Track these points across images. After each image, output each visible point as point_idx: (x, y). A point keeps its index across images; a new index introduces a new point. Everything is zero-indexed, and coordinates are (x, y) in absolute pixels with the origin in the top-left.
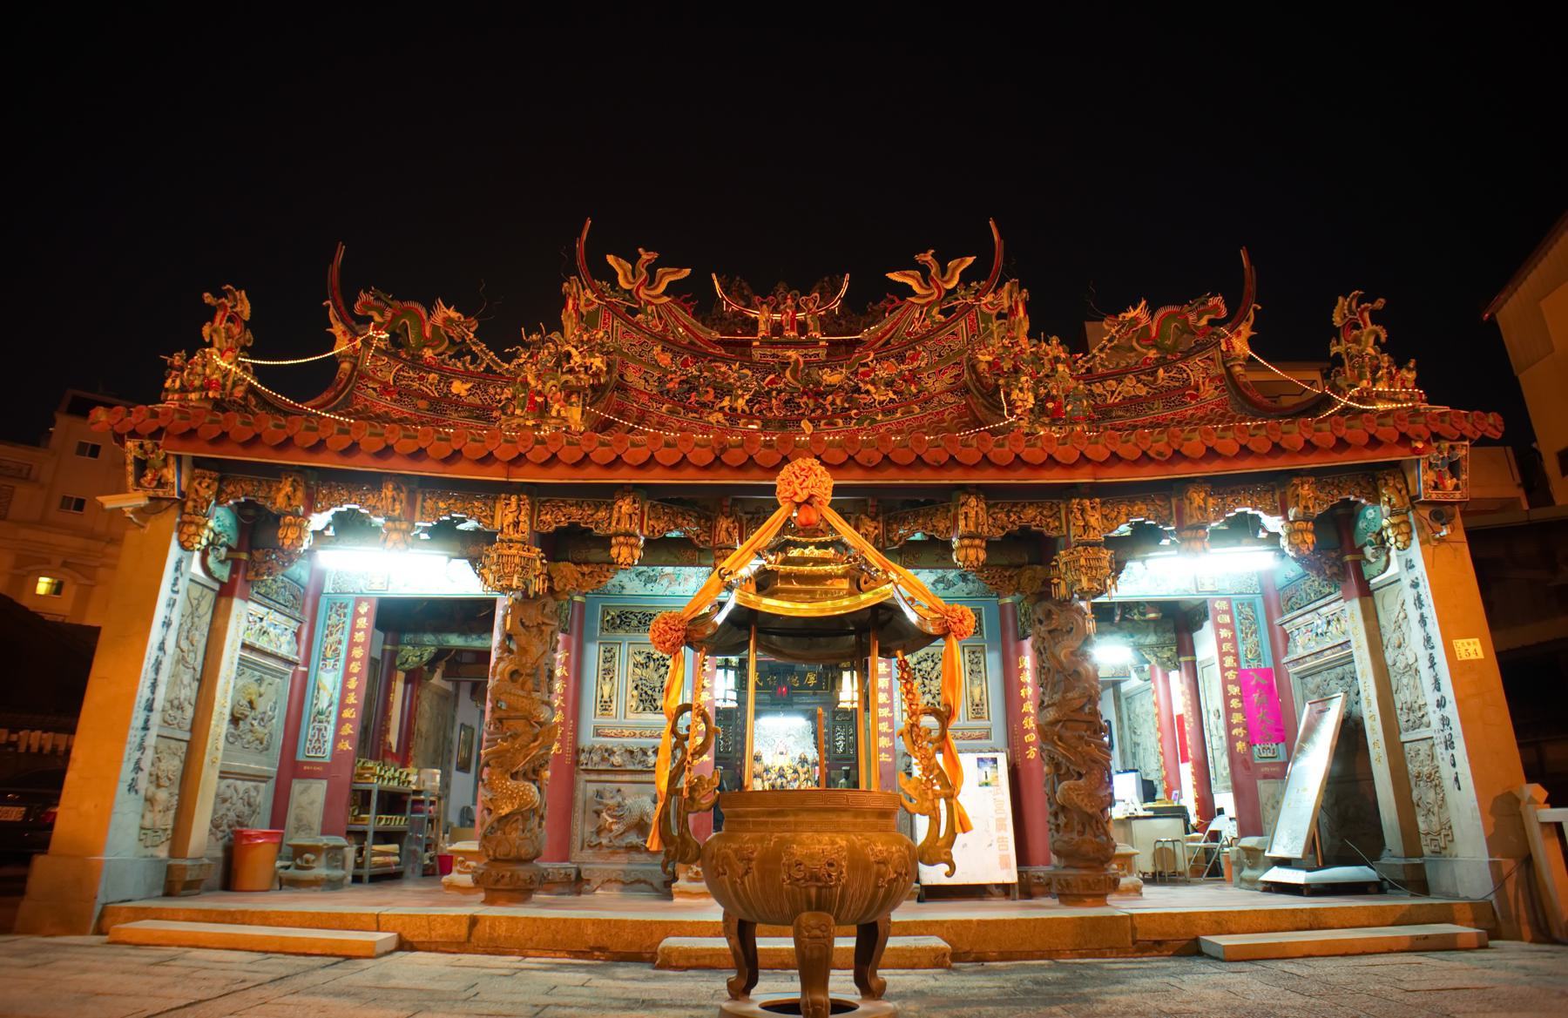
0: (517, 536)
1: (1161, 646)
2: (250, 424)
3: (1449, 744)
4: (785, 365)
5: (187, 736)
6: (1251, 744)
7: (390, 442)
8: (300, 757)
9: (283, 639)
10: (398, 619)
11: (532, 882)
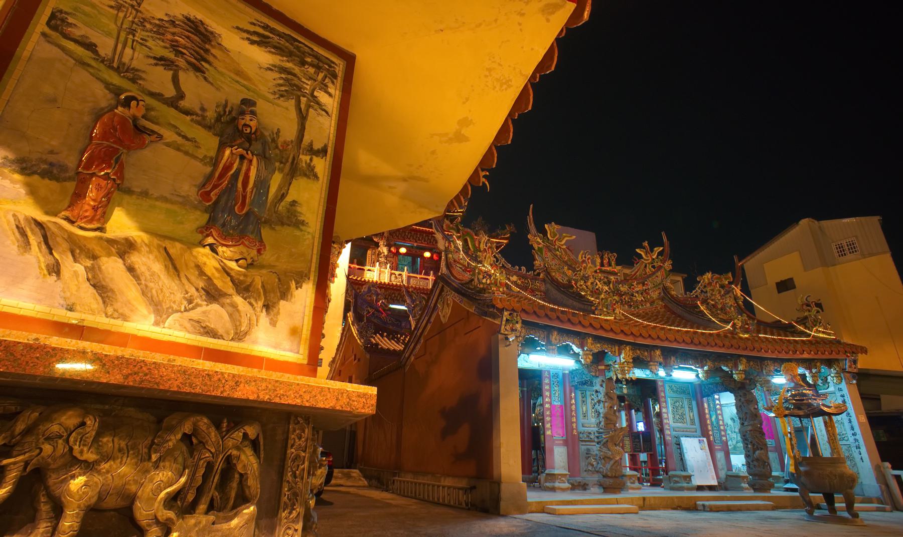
3: (858, 447)
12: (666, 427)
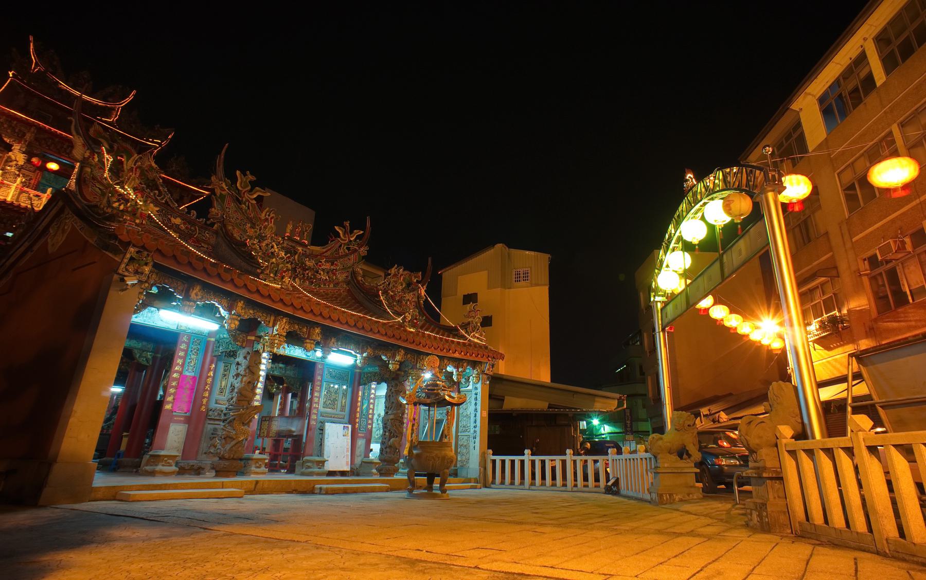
3: (475, 438)
12: (315, 411)
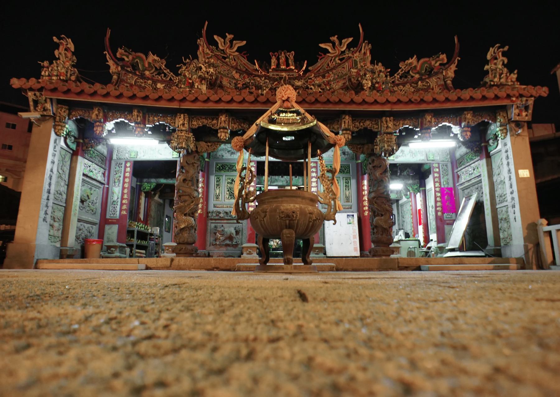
0: (184, 129)
1: (414, 184)
2: (78, 86)
3: (514, 206)
4: (281, 78)
5: (64, 205)
6: (443, 213)
7: (135, 93)
8: (108, 217)
9: (98, 175)
10: (143, 169)
11: (192, 251)
